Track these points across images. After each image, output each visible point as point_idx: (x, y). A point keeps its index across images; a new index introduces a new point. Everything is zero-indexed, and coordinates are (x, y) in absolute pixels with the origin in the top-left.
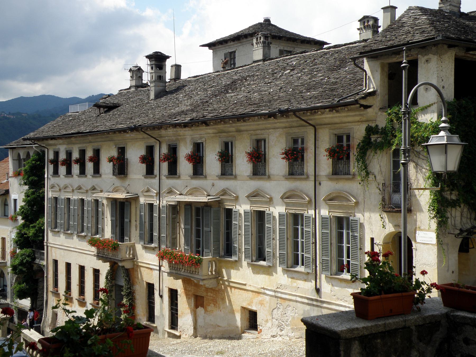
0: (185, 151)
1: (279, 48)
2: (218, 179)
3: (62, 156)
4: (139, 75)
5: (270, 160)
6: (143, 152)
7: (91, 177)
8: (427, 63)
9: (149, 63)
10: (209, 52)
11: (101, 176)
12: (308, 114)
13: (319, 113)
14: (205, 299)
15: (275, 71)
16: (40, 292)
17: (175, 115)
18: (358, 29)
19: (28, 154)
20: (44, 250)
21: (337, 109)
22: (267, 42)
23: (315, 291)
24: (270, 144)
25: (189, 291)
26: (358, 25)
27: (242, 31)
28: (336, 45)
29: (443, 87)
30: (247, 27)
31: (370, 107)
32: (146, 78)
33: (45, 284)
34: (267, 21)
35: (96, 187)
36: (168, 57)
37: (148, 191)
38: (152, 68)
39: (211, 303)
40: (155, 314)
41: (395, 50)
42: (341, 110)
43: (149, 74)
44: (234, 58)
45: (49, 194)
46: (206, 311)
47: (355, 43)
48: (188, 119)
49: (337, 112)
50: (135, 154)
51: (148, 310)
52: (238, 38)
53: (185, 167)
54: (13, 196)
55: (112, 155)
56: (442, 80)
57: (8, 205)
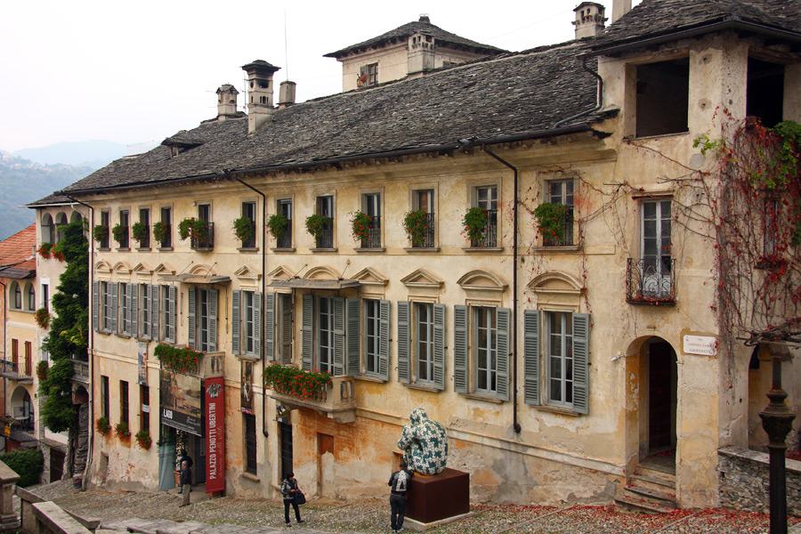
0: (303, 211)
1: (443, 60)
2: (356, 253)
3: (115, 221)
4: (231, 99)
5: (441, 223)
6: (237, 214)
7: (158, 251)
8: (705, 63)
9: (247, 77)
10: (336, 65)
11: (173, 249)
12: (506, 148)
13: (524, 146)
14: (335, 439)
15: (444, 88)
16: (81, 425)
17: (289, 154)
18: (573, 23)
19: (64, 218)
20: (87, 361)
21: (554, 139)
22: (429, 44)
23: (512, 430)
24: (441, 198)
25: (310, 427)
26: (573, 17)
27: (387, 34)
28: (539, 48)
29: (731, 102)
30: (394, 27)
31: (608, 135)
32: (242, 103)
33: (90, 417)
34: (425, 20)
35: (165, 266)
36: (277, 69)
37: (246, 271)
38: (252, 86)
39: (344, 447)
40: (258, 461)
41: (652, 41)
42: (561, 140)
43: (247, 95)
44: (376, 73)
45: (97, 276)
46: (337, 458)
47: (570, 43)
48: (308, 160)
49: (554, 143)
50: (225, 217)
51: (246, 455)
52: (381, 43)
53: (303, 237)
54: (42, 279)
55: (189, 217)
56: (730, 91)
57: (34, 294)
